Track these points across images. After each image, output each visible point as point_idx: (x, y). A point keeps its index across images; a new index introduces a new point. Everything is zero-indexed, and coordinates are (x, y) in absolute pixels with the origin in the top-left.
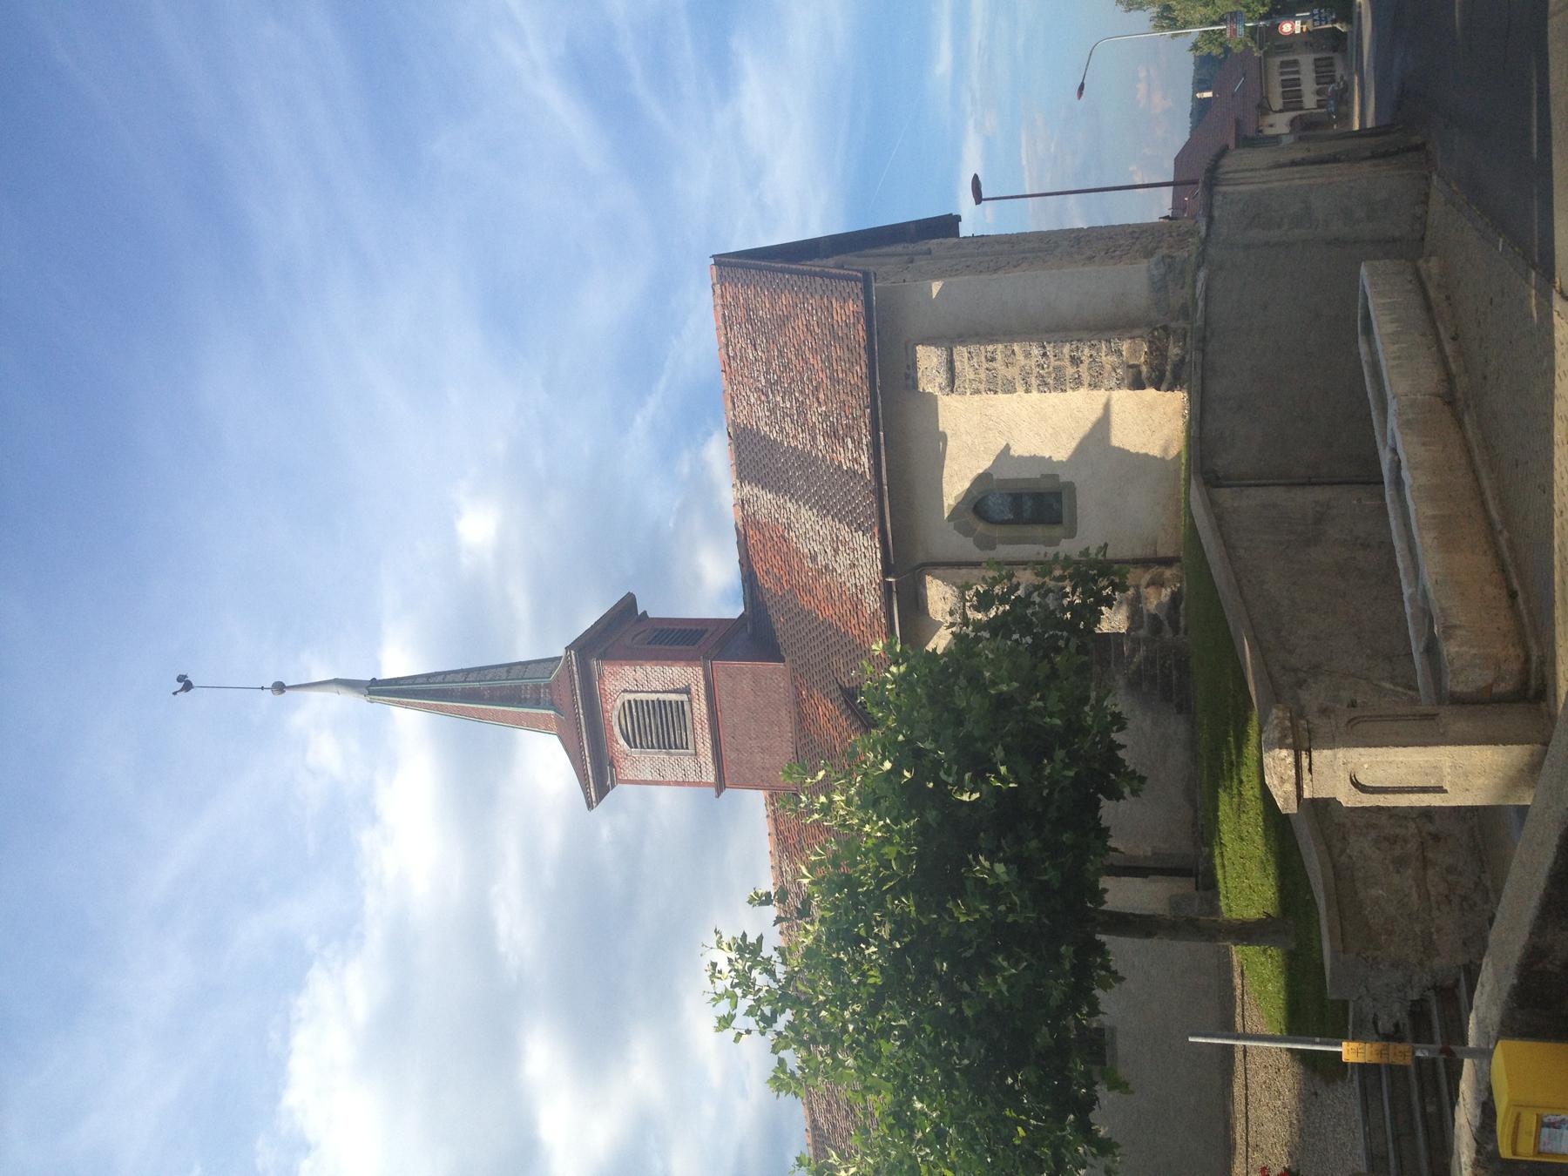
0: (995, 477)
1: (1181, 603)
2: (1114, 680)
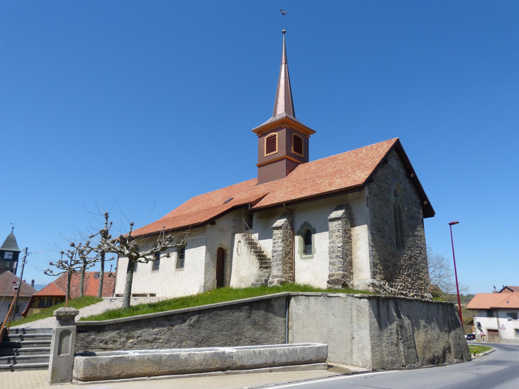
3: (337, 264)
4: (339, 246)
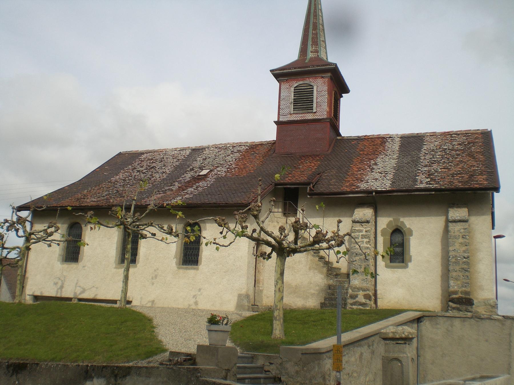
0: (411, 237)
1: (362, 307)
2: (330, 280)
3: (461, 278)
4: (466, 257)
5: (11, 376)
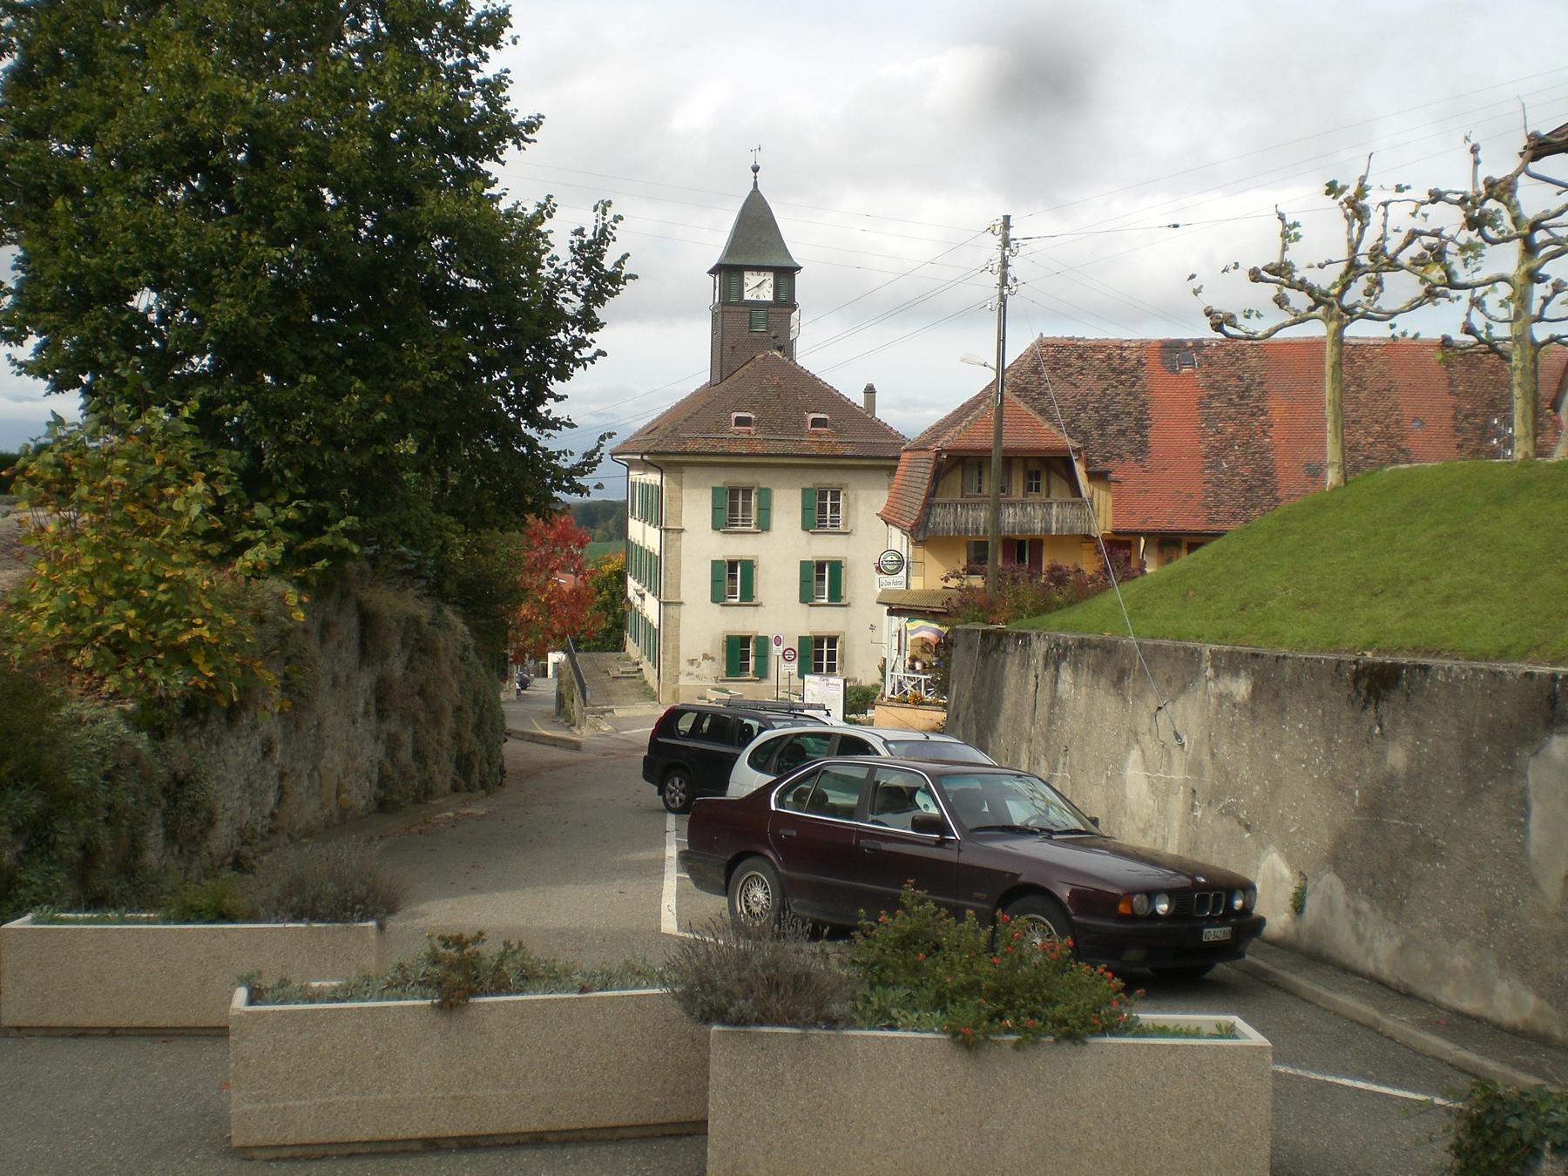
5: (1365, 708)
